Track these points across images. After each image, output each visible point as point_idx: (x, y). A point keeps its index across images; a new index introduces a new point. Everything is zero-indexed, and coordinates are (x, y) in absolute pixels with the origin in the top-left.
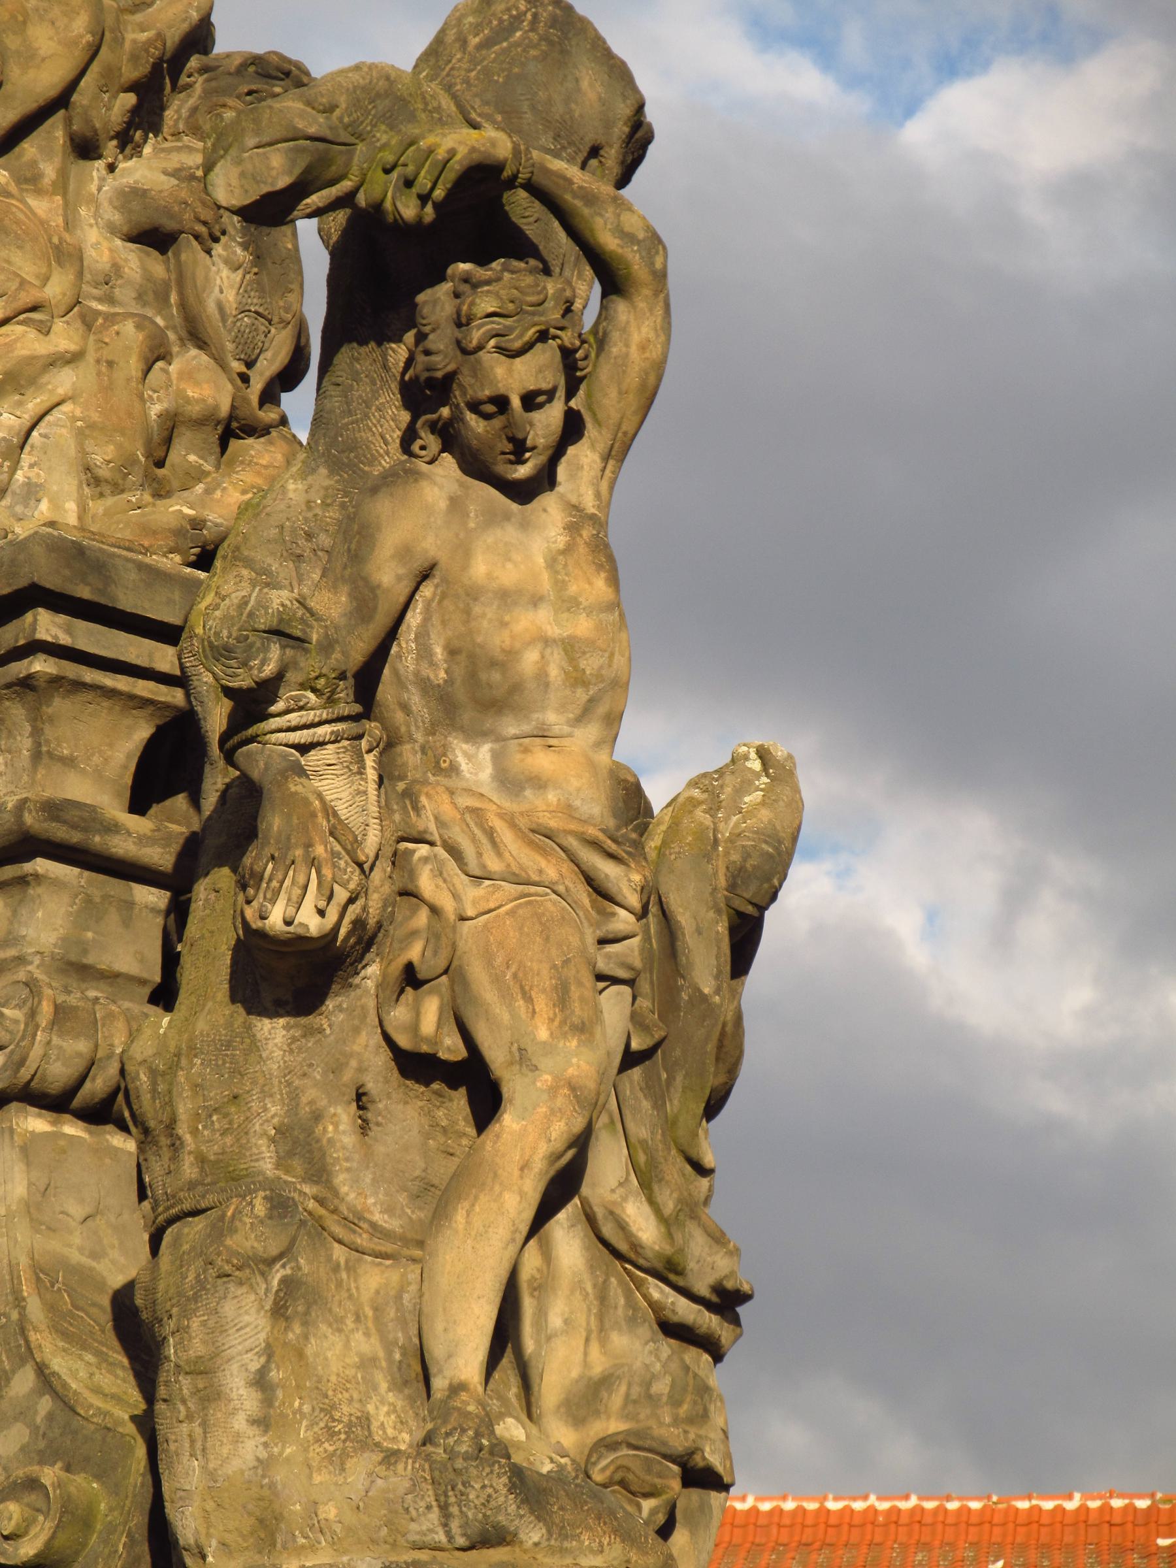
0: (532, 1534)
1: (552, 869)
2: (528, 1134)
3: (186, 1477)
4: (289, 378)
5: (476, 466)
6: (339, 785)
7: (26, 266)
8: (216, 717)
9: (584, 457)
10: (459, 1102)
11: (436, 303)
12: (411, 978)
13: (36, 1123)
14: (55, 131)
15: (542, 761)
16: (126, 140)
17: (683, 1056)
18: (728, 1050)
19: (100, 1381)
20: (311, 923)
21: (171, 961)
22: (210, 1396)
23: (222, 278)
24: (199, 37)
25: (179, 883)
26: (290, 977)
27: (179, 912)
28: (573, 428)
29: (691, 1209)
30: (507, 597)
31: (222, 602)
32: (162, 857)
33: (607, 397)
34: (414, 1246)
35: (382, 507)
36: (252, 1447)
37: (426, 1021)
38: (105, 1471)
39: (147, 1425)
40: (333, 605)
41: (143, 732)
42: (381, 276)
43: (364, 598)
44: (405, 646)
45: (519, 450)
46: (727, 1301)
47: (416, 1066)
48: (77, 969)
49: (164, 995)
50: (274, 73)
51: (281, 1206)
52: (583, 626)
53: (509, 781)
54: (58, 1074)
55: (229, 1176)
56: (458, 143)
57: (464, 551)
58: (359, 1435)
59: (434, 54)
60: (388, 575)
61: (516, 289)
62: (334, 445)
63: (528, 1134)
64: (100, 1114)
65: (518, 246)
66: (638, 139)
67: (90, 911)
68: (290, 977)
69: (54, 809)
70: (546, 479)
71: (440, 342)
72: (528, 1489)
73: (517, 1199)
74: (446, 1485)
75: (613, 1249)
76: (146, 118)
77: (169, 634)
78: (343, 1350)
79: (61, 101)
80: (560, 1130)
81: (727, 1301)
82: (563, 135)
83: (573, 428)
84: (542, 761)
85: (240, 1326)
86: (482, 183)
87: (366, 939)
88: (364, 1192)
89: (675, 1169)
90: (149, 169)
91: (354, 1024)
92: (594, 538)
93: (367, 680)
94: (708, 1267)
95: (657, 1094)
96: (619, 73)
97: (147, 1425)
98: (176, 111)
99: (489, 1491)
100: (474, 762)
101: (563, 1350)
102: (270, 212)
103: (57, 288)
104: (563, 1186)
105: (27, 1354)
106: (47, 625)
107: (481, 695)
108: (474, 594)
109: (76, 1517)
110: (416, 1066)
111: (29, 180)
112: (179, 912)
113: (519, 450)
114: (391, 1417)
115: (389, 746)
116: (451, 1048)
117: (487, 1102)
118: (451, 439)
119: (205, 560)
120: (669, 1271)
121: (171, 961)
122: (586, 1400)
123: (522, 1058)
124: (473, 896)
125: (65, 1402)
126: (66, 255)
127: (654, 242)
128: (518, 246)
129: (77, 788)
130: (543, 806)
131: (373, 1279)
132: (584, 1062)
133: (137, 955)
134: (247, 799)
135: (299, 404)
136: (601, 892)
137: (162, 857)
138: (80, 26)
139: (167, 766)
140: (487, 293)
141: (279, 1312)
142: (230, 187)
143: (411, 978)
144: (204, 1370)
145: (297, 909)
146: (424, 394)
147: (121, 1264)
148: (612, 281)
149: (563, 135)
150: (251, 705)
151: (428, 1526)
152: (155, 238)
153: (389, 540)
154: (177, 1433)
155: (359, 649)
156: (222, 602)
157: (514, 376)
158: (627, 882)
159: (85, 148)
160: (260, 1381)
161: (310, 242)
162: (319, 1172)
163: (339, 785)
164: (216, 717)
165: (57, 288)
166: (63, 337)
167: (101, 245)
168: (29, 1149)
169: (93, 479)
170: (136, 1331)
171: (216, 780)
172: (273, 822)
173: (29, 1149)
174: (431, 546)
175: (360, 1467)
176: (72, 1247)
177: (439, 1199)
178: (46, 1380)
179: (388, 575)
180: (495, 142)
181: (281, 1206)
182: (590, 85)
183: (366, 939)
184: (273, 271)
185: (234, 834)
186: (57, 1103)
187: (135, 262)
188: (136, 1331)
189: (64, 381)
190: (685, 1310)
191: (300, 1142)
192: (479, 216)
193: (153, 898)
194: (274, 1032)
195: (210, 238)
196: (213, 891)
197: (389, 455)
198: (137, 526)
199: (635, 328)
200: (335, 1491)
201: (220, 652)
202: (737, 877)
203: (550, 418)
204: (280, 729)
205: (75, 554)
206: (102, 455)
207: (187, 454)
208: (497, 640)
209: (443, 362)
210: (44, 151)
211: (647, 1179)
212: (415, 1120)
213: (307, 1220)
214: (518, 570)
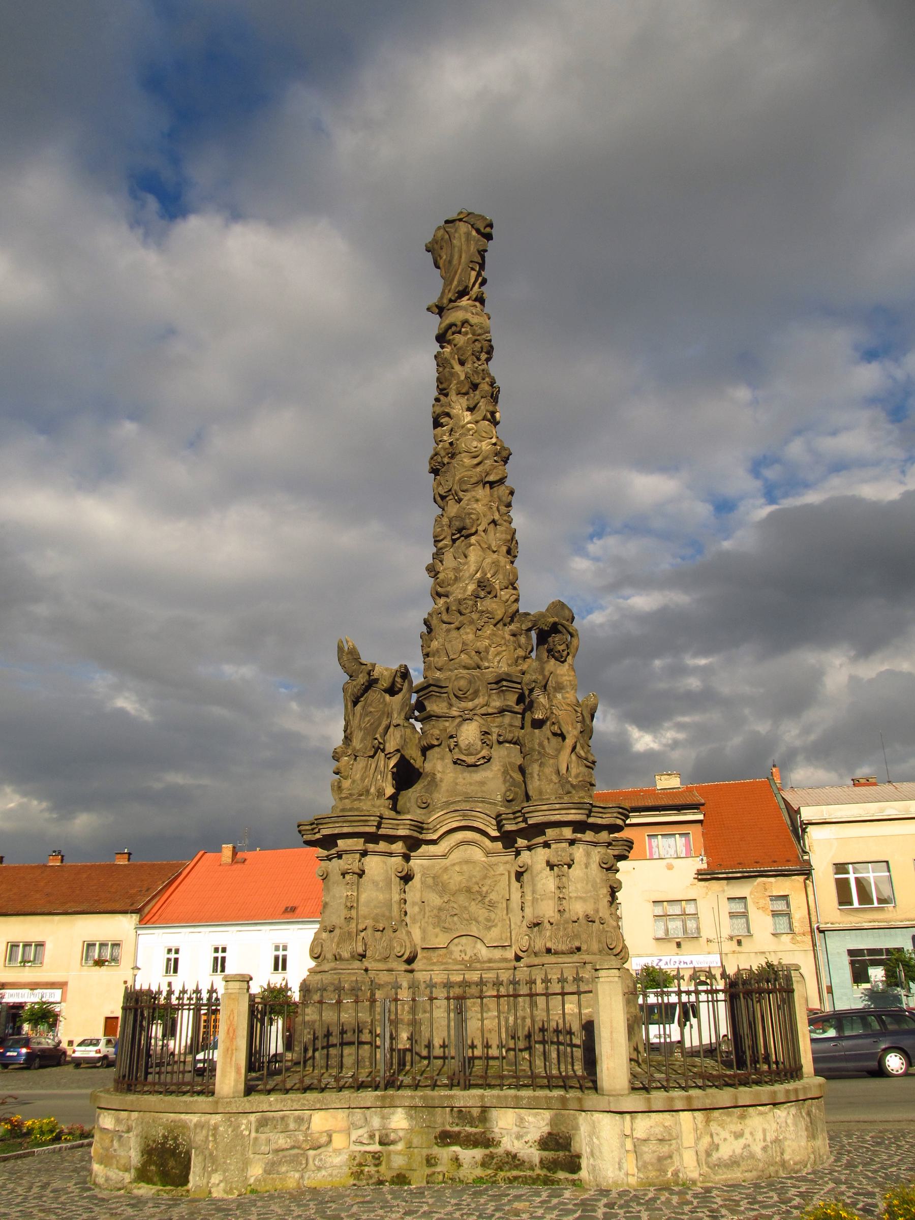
0: (574, 792)
1: (570, 708)
2: (569, 742)
3: (530, 787)
4: (531, 651)
5: (556, 659)
6: (543, 700)
7: (499, 640)
8: (527, 693)
9: (570, 657)
10: (560, 739)
11: (550, 639)
12: (554, 723)
13: (507, 745)
14: (501, 623)
15: (567, 695)
16: (510, 624)
17: (587, 732)
18: (591, 731)
19: (518, 777)
20: (541, 717)
21: (523, 724)
22: (532, 777)
23: (523, 639)
24: (517, 611)
25: (523, 714)
26: (538, 724)
27: (523, 718)
28: (568, 654)
29: (588, 751)
30: (562, 675)
31: (526, 678)
32: (521, 711)
33: (572, 650)
34: (556, 757)
35: (545, 665)
36: (538, 783)
37: (556, 728)
38: (519, 788)
39: (524, 782)
40: (540, 677)
41: (517, 696)
42: (543, 637)
43: (544, 676)
44: (550, 682)
45: (562, 657)
46: (594, 763)
47: (555, 734)
48: (511, 726)
49: (522, 728)
50: (527, 614)
51: (539, 753)
52: (571, 678)
53: (564, 698)
54: (510, 738)
55: (533, 749)
56: (551, 620)
57: (556, 670)
58: (551, 781)
59: (547, 610)
60: (547, 673)
61: (103, 1200)
62: (538, 658)
63: (569, 742)
64: (515, 743)
65: (560, 632)
66: (573, 618)
67: (512, 718)
68: (538, 724)
69: (507, 706)
70: (565, 660)
71: (551, 644)
72: (573, 786)
73: (569, 750)
74: (563, 786)
75: (579, 757)
76: (512, 621)
77: (519, 683)
78: (548, 770)
79: (502, 619)
80: (573, 741)
81: (594, 763)
82: (564, 619)
83: (568, 654)
84: (567, 695)
85: (535, 769)
86: (555, 625)
87: (547, 719)
88: (550, 751)
89: (586, 746)
90: (513, 627)
91: (546, 729)
92: (572, 667)
93: (545, 686)
94: (591, 758)
95: (583, 737)
96: (570, 610)
97: (524, 782)
98: (515, 620)
99: (568, 787)
100: (559, 696)
101: (574, 771)
102: (529, 630)
103: (503, 642)
104: (574, 748)
105: (508, 774)
106: (505, 683)
107: (559, 688)
108: (557, 675)
109: (516, 793)
110: (555, 734)
111: (498, 629)
112: (523, 718)
113: (562, 657)
114: (555, 778)
115: (548, 695)
116: (559, 732)
117: (564, 738)
118: (553, 656)
119: (523, 674)
120: (586, 759)
121: (523, 724)
122: (577, 776)
123: (568, 732)
124: (561, 713)
125: (514, 779)
126: (504, 638)
127: (576, 630)
128: (560, 632)
129: (509, 703)
130: (568, 701)
131: (551, 761)
132: (576, 732)
133: (518, 723)
134: (531, 703)
135: (533, 655)
136: (576, 711)
137: (521, 711)
138: (503, 611)
139: (521, 699)
140: (557, 638)
141: (540, 766)
142: (524, 627)
143: (554, 723)
144: (531, 774)
145: (539, 716)
146: (549, 651)
147: (519, 761)
148: (572, 636)
149: (564, 619)
150: (531, 691)
151: (561, 791)
152: (514, 635)
153: (547, 669)
154: (528, 782)
155: (544, 683)
156: (526, 678)
157: (560, 648)
158: (579, 709)
159: (505, 625)
160: (538, 775)
161: (533, 634)
162: (544, 748)
163: (543, 700)
164: (527, 693)
165: (503, 642)
166: (504, 648)
167: (507, 637)
168: (507, 748)
169: (509, 665)
170: (522, 770)
171: (527, 700)
172: (535, 705)
173: (507, 748)
174: (552, 670)
175: (552, 785)
176: (513, 760)
177: (559, 751)
178: (511, 777)
179: (547, 673)
180: (556, 619)
181: (539, 753)
182: (567, 612)
183: (547, 719)
184: (529, 638)
185: (530, 707)
186: (510, 742)
187: (512, 638)
188: (522, 770)
189: (504, 653)
190: (589, 764)
191: (541, 745)
192: (555, 629)
193: (520, 716)
194: (537, 731)
195: (521, 635)
196: (528, 714)
197: (546, 659)
198: (514, 670)
199: (575, 641)
200: (548, 788)
201: (527, 684)
202: (591, 709)
203: (565, 653)
204: (535, 693)
205: (508, 674)
206: (510, 662)
207: (520, 661)
208: (560, 680)
209: (552, 647)
210: (500, 626)
211: (583, 748)
212: (555, 741)
213: (542, 754)
214: (563, 672)
